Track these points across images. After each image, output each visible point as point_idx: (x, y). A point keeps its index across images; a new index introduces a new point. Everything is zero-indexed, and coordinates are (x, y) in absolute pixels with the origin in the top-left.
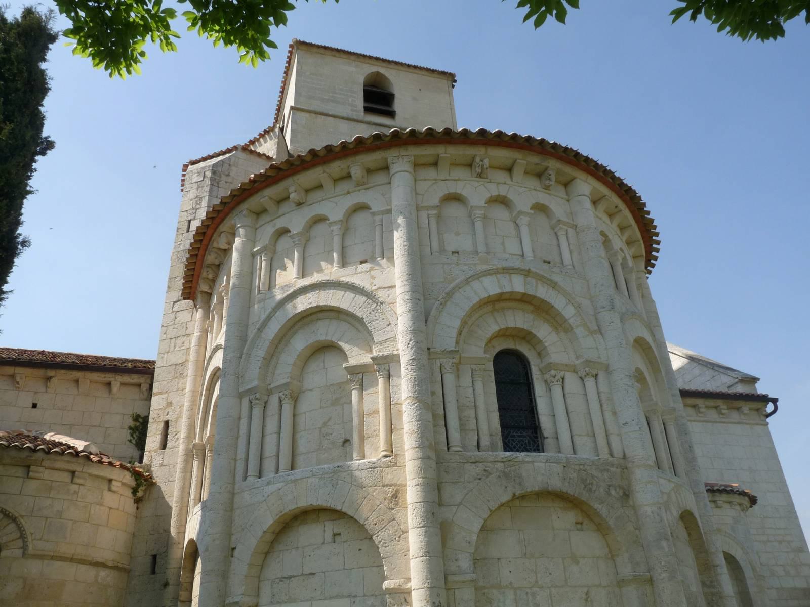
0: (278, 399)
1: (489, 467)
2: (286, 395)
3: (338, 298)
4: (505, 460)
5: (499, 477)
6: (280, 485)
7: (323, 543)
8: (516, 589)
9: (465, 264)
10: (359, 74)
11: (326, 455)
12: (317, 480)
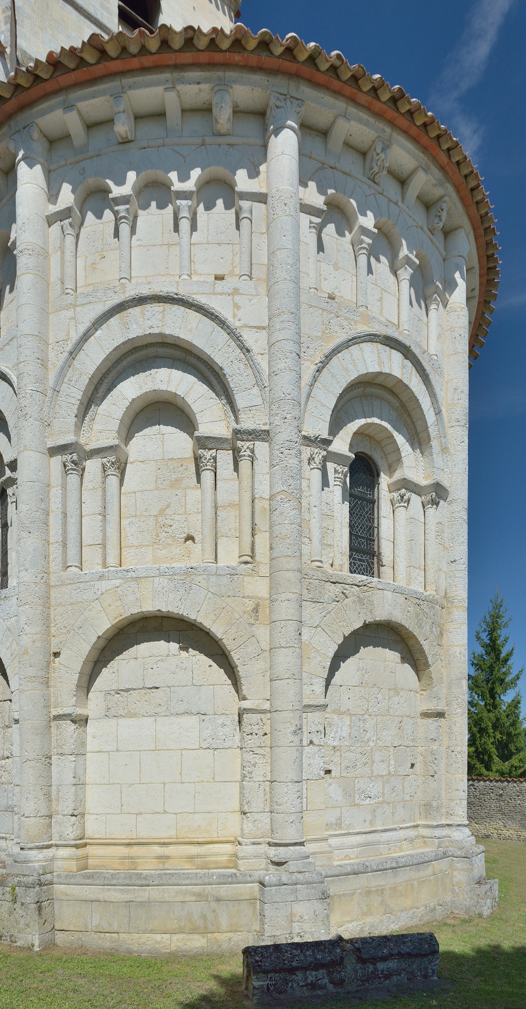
0: (101, 467)
1: (346, 589)
2: (113, 463)
3: (189, 328)
4: (361, 584)
5: (354, 601)
6: (117, 582)
7: (168, 656)
8: (351, 715)
9: (346, 319)
11: (163, 552)
12: (166, 581)
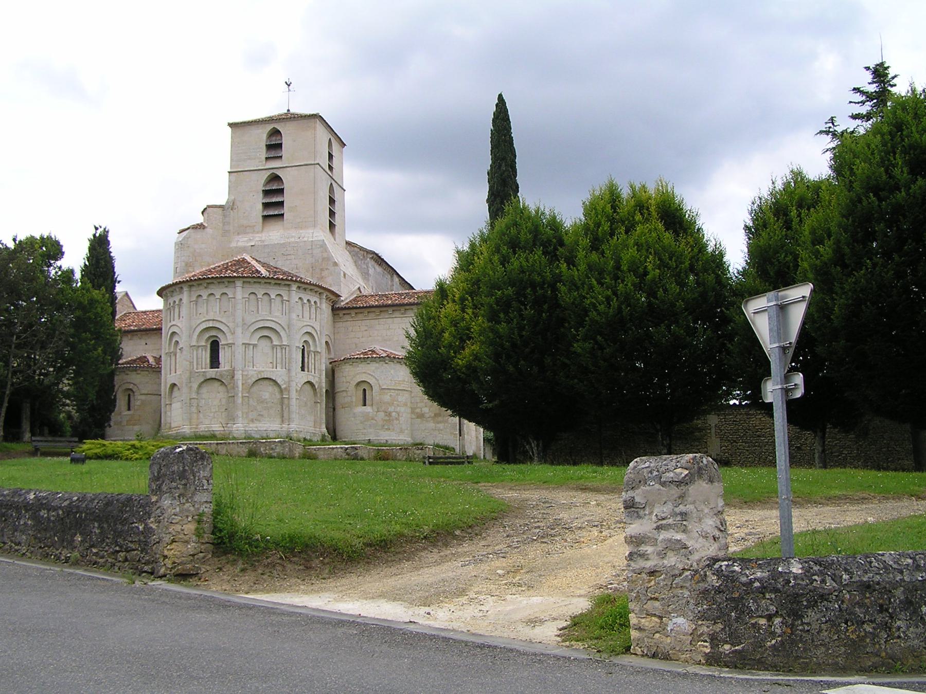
10: (261, 136)
